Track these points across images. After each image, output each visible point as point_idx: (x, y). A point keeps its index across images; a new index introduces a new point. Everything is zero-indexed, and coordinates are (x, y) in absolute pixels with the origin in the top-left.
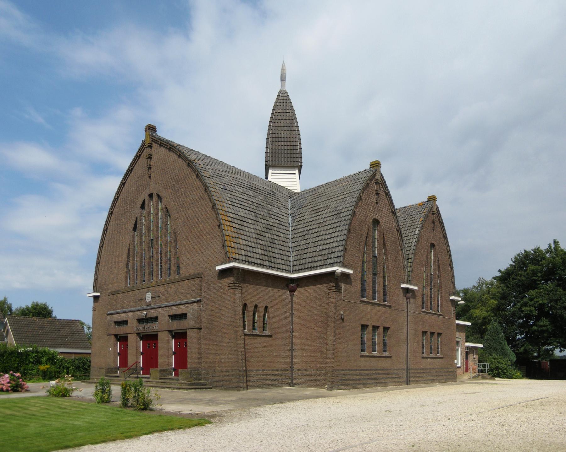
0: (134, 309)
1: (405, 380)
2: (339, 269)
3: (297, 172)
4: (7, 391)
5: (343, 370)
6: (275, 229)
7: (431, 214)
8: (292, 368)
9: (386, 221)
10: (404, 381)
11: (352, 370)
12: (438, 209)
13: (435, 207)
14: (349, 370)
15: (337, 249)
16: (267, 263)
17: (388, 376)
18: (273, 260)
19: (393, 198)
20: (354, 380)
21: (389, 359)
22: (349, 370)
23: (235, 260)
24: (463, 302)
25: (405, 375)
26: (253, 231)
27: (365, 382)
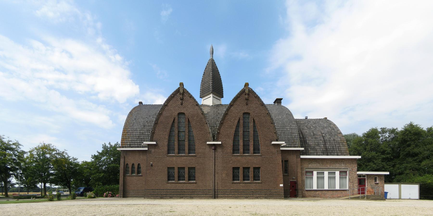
14: (157, 190)
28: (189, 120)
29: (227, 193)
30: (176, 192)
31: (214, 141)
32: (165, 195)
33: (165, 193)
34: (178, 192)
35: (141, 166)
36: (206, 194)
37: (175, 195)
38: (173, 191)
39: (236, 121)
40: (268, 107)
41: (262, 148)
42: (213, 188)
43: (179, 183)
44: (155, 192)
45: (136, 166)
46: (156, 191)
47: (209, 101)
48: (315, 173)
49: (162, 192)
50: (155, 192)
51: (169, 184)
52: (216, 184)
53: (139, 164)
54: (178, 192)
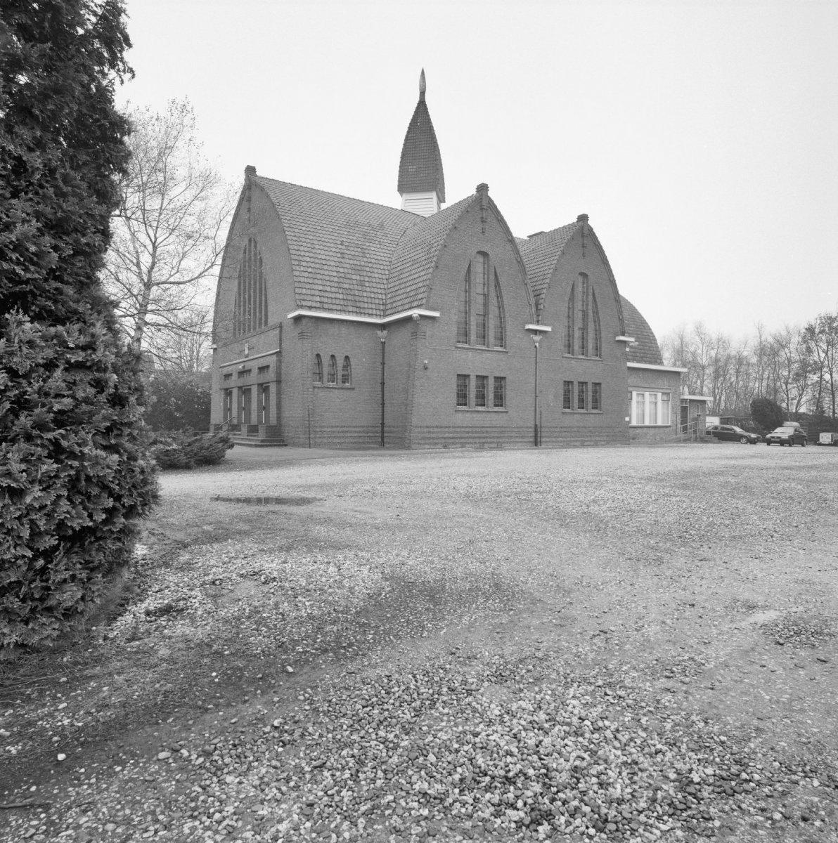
0: (238, 361)
1: (532, 440)
2: (415, 313)
3: (434, 195)
4: (722, 436)
5: (427, 427)
6: (368, 269)
7: (581, 237)
8: (383, 424)
9: (498, 252)
10: (530, 442)
11: (441, 427)
12: (591, 230)
13: (586, 228)
14: (437, 427)
15: (422, 290)
16: (351, 309)
17: (502, 435)
18: (358, 305)
19: (509, 224)
20: (445, 438)
21: (504, 415)
22: (437, 427)
23: (302, 307)
24: (637, 343)
25: (532, 434)
26: (335, 274)
27: (462, 440)
28: (495, 272)
29: (555, 435)
30: (472, 432)
31: (538, 322)
32: (451, 441)
33: (451, 435)
34: (476, 432)
35: (353, 361)
36: (522, 437)
37: (470, 440)
38: (467, 430)
39: (569, 289)
40: (519, 247)
41: (605, 348)
42: (531, 424)
43: (478, 412)
44: (433, 433)
45: (340, 362)
46: (436, 430)
47: (424, 205)
48: (634, 394)
49: (445, 433)
50: (433, 433)
51: (460, 414)
52: (538, 416)
53: (347, 357)
54: (476, 432)
